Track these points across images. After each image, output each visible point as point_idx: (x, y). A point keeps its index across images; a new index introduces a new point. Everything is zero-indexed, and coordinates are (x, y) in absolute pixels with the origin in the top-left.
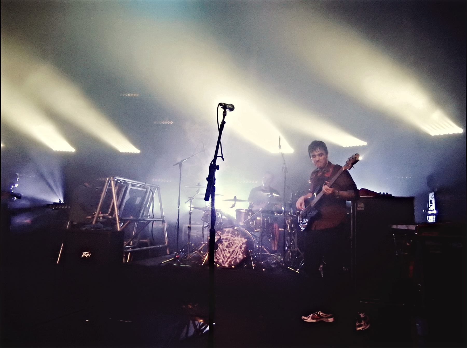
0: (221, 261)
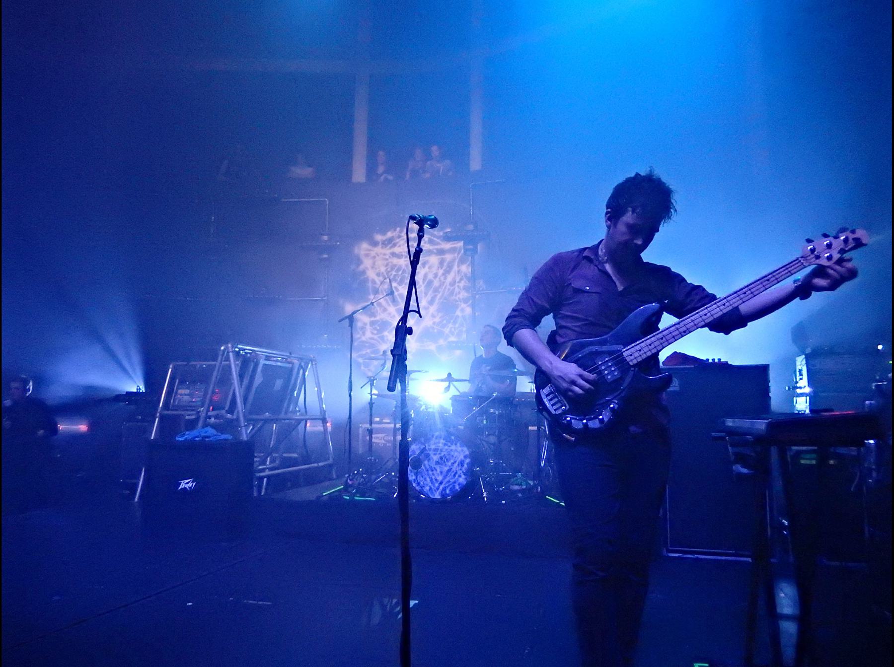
0: (428, 488)
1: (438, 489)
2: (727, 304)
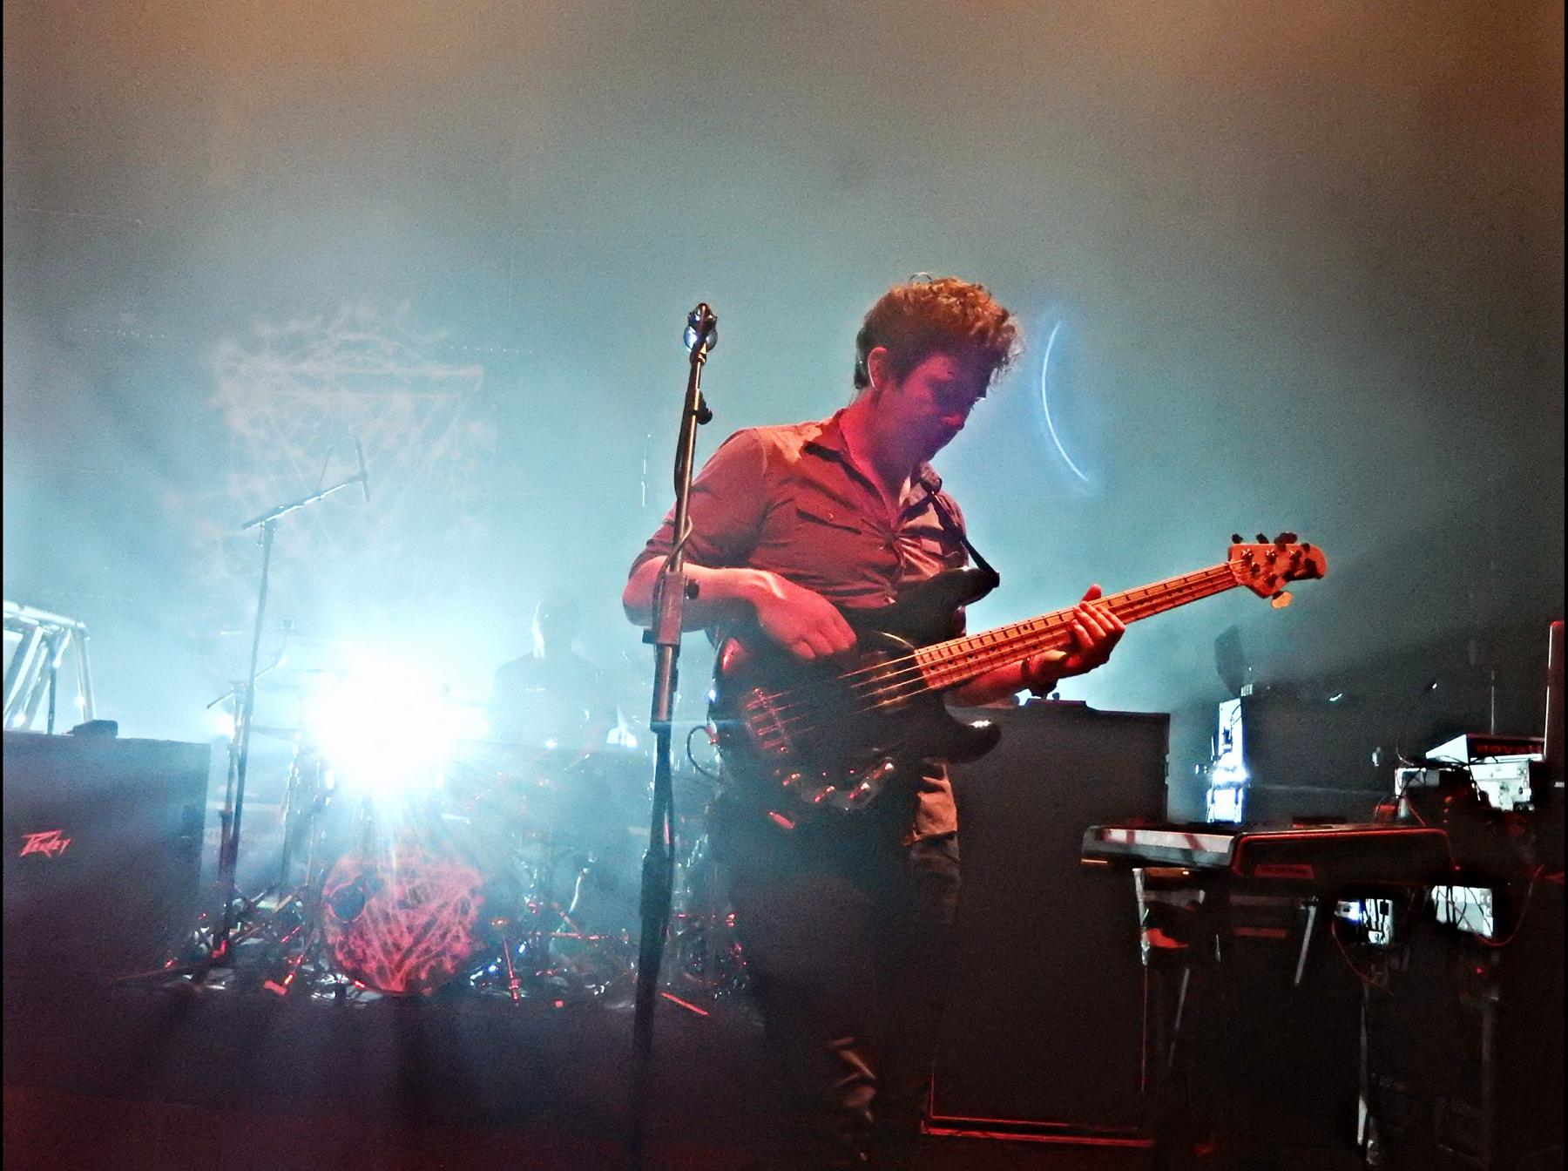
0: (373, 965)
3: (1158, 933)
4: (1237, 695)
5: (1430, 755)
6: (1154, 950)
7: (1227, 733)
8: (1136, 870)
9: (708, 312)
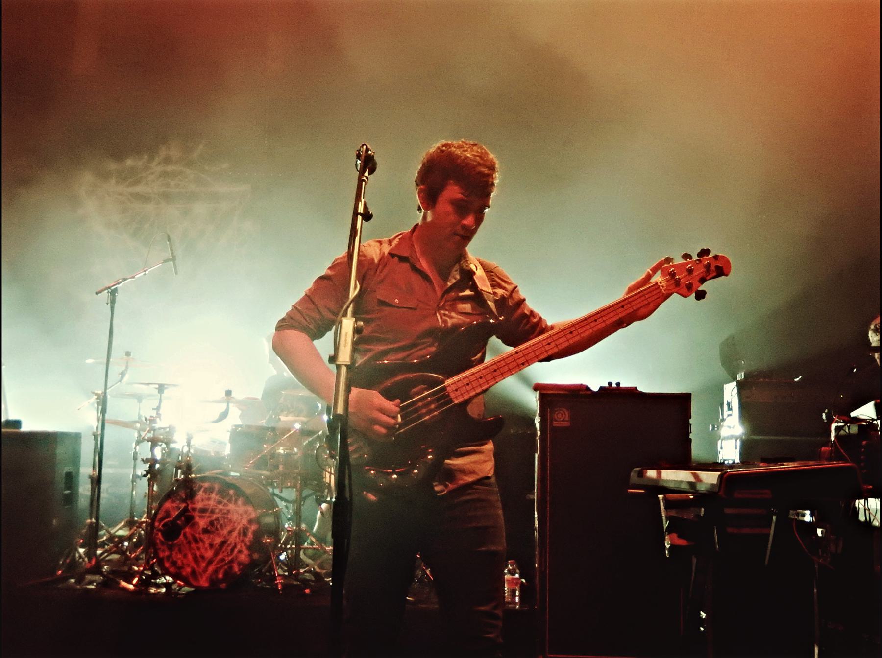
0: (189, 570)
1: (205, 570)
2: (575, 333)
3: (675, 535)
4: (735, 379)
5: (853, 414)
6: (673, 547)
7: (729, 404)
8: (661, 496)
9: (367, 150)
